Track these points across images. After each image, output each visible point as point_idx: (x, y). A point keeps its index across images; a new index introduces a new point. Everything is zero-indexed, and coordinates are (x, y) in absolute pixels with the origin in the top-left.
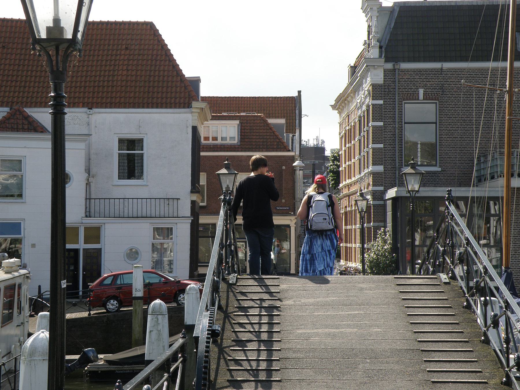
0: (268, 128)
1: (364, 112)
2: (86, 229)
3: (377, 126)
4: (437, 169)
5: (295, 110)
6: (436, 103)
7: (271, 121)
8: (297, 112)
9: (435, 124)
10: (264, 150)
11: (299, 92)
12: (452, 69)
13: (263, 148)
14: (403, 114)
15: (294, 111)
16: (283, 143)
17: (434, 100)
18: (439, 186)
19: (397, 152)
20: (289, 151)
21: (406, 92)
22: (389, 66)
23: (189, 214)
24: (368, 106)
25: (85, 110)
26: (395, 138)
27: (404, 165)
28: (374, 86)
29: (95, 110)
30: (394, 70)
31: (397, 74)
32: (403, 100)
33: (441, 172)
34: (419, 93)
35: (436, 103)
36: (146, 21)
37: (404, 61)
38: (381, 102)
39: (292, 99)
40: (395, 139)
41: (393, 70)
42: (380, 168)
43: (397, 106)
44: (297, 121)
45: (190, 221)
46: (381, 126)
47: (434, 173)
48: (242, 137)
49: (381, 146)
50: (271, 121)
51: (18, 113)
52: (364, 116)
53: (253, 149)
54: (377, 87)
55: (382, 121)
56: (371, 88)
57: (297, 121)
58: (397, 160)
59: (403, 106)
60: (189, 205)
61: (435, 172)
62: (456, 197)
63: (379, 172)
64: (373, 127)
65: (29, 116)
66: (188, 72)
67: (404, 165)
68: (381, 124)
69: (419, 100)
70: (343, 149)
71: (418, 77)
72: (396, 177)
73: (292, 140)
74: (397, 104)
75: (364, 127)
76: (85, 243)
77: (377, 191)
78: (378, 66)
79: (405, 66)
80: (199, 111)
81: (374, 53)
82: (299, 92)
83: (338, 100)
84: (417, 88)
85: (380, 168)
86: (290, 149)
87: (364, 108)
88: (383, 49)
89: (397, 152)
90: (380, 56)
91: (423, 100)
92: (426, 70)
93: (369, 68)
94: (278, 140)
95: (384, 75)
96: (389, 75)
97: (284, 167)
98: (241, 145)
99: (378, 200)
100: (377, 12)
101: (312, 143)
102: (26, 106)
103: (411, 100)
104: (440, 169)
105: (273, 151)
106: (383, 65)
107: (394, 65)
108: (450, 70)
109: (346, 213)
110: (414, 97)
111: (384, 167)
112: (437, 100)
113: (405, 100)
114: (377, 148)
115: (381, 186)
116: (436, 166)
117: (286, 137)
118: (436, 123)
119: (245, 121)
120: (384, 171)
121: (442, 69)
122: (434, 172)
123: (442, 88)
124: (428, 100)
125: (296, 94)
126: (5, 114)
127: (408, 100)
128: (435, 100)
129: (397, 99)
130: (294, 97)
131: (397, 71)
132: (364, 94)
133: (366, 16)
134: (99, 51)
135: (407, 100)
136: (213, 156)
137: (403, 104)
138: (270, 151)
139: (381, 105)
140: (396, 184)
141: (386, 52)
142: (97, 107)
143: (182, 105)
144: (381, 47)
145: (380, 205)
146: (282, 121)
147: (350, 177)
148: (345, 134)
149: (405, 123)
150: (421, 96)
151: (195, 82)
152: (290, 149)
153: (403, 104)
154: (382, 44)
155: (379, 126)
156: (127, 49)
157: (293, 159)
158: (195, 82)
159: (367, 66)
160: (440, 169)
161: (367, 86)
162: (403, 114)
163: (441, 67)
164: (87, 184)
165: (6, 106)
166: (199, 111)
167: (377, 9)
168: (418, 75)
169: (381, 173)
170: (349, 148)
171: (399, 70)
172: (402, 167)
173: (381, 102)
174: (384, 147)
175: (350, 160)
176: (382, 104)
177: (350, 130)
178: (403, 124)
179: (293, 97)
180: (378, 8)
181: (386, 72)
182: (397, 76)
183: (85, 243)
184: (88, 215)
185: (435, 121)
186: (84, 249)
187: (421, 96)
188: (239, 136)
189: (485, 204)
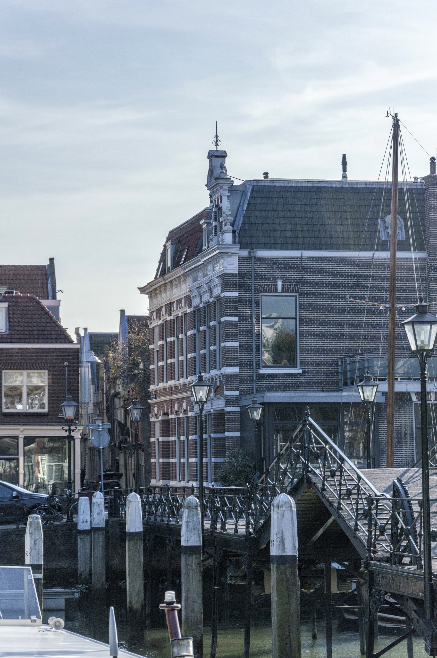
0: (43, 312)
3: (231, 321)
4: (298, 371)
5: (47, 284)
6: (296, 296)
8: (50, 286)
9: (294, 320)
10: (40, 341)
11: (52, 260)
13: (25, 338)
14: (260, 308)
15: (45, 286)
17: (294, 292)
18: (313, 390)
19: (254, 351)
21: (263, 283)
22: (245, 253)
26: (252, 335)
27: (261, 366)
30: (250, 258)
31: (253, 263)
32: (260, 292)
33: (302, 374)
34: (277, 285)
35: (296, 296)
36: (161, 252)
37: (259, 248)
39: (42, 268)
40: (252, 337)
41: (248, 258)
43: (253, 299)
46: (236, 321)
47: (295, 375)
48: (11, 324)
53: (26, 340)
54: (231, 277)
55: (237, 316)
59: (260, 298)
61: (276, 374)
62: (343, 403)
63: (232, 374)
67: (261, 366)
69: (276, 291)
71: (275, 266)
72: (253, 380)
74: (253, 296)
77: (232, 395)
78: (232, 253)
79: (261, 253)
82: (52, 260)
84: (276, 279)
88: (237, 234)
89: (254, 351)
90: (234, 242)
91: (282, 292)
92: (285, 259)
93: (222, 255)
94: (57, 329)
95: (239, 263)
96: (244, 264)
98: (10, 334)
99: (233, 407)
100: (228, 191)
103: (268, 292)
104: (301, 371)
105: (61, 342)
106: (238, 252)
107: (249, 252)
108: (310, 259)
111: (240, 369)
112: (297, 293)
113: (262, 292)
114: (231, 346)
115: (237, 390)
118: (296, 319)
119: (14, 304)
120: (240, 373)
121: (301, 258)
122: (288, 374)
123: (302, 279)
124: (290, 292)
125: (46, 263)
127: (265, 292)
128: (295, 293)
129: (253, 291)
130: (45, 266)
131: (253, 259)
135: (264, 292)
137: (260, 296)
138: (48, 343)
140: (253, 387)
141: (239, 236)
144: (234, 232)
145: (235, 412)
150: (280, 288)
153: (260, 296)
154: (235, 228)
155: (234, 321)
160: (301, 371)
162: (260, 308)
163: (301, 255)
167: (227, 188)
168: (276, 264)
169: (237, 375)
171: (255, 258)
172: (260, 369)
174: (239, 346)
176: (237, 297)
178: (260, 319)
179: (43, 266)
180: (228, 187)
181: (240, 259)
182: (253, 265)
185: (294, 316)
187: (280, 288)
188: (8, 324)
189: (175, 427)
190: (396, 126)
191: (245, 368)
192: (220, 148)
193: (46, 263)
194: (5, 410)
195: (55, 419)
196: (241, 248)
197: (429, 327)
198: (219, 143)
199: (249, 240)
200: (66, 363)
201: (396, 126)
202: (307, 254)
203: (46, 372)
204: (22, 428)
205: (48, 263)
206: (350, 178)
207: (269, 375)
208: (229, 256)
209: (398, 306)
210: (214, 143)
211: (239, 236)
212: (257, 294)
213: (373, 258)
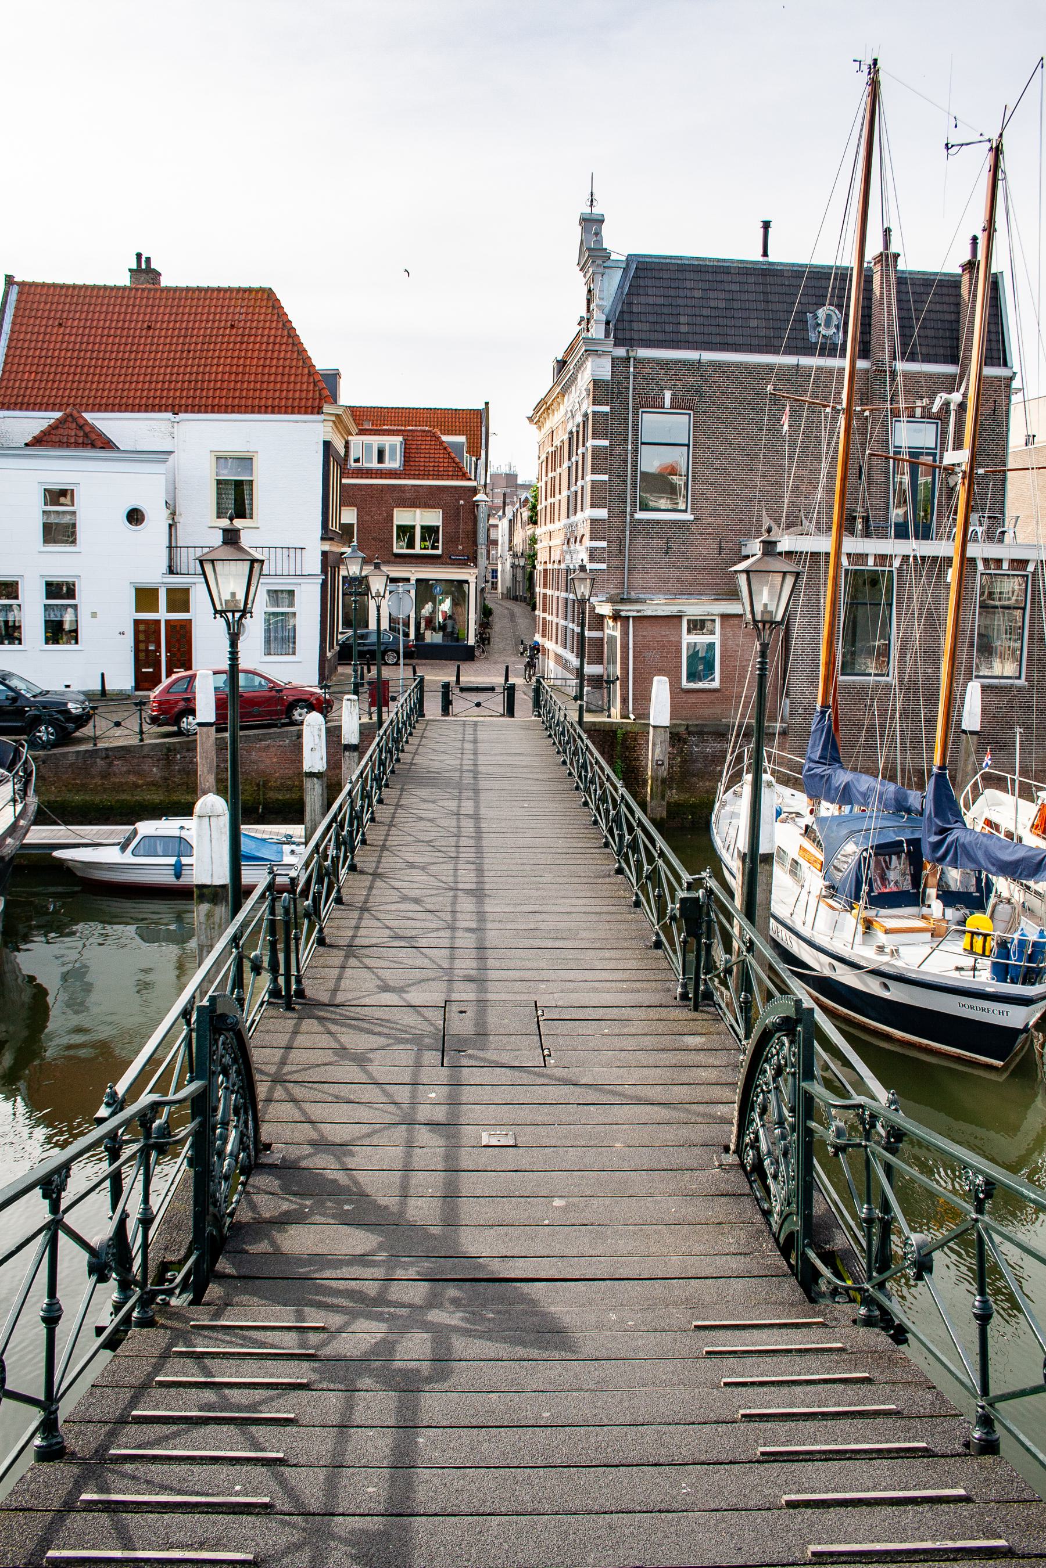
1: (578, 426)
2: (169, 591)
6: (689, 414)
7: (445, 438)
8: (483, 429)
11: (487, 404)
12: (715, 362)
16: (461, 469)
20: (470, 479)
22: (621, 352)
23: (317, 570)
24: (586, 415)
25: (169, 415)
28: (596, 382)
29: (182, 416)
35: (689, 414)
38: (606, 409)
39: (478, 412)
42: (602, 513)
44: (483, 441)
45: (320, 581)
47: (684, 522)
49: (606, 477)
50: (445, 438)
51: (70, 419)
52: (578, 432)
56: (591, 386)
57: (483, 441)
58: (629, 501)
60: (319, 558)
64: (594, 447)
65: (93, 428)
66: (321, 362)
68: (606, 443)
70: (544, 478)
71: (663, 372)
73: (476, 465)
75: (577, 449)
76: (168, 611)
79: (643, 353)
80: (333, 418)
81: (597, 331)
82: (487, 404)
83: (537, 409)
85: (602, 513)
86: (473, 477)
87: (579, 419)
90: (607, 335)
92: (676, 362)
97: (462, 502)
101: (504, 470)
102: (86, 411)
108: (711, 363)
109: (545, 571)
110: (656, 404)
116: (685, 511)
117: (467, 461)
118: (688, 445)
125: (482, 406)
126: (53, 421)
132: (579, 396)
133: (585, 276)
134: (193, 329)
136: (388, 485)
139: (606, 414)
142: (186, 412)
143: (310, 410)
146: (462, 439)
147: (552, 521)
148: (547, 458)
149: (642, 443)
150: (667, 402)
151: (332, 378)
152: (473, 477)
156: (232, 326)
157: (474, 491)
158: (332, 378)
159: (586, 351)
160: (692, 517)
161: (584, 380)
164: (170, 526)
165: (59, 411)
166: (333, 418)
170: (553, 479)
173: (606, 409)
175: (553, 495)
177: (554, 453)
181: (614, 360)
182: (632, 369)
183: (168, 611)
184: (171, 571)
186: (167, 621)
187: (667, 402)
190: (874, 85)
191: (617, 511)
192: (595, 211)
193: (482, 406)
194: (396, 551)
195: (448, 561)
196: (615, 345)
197: (241, 676)
198: (595, 203)
199: (627, 335)
200: (462, 502)
201: (874, 85)
202: (707, 356)
203: (441, 511)
204: (413, 570)
205: (483, 406)
206: (772, 258)
207: (648, 521)
208: (600, 356)
209: (858, 409)
210: (589, 203)
211: (615, 330)
212: (636, 414)
213: (798, 365)
